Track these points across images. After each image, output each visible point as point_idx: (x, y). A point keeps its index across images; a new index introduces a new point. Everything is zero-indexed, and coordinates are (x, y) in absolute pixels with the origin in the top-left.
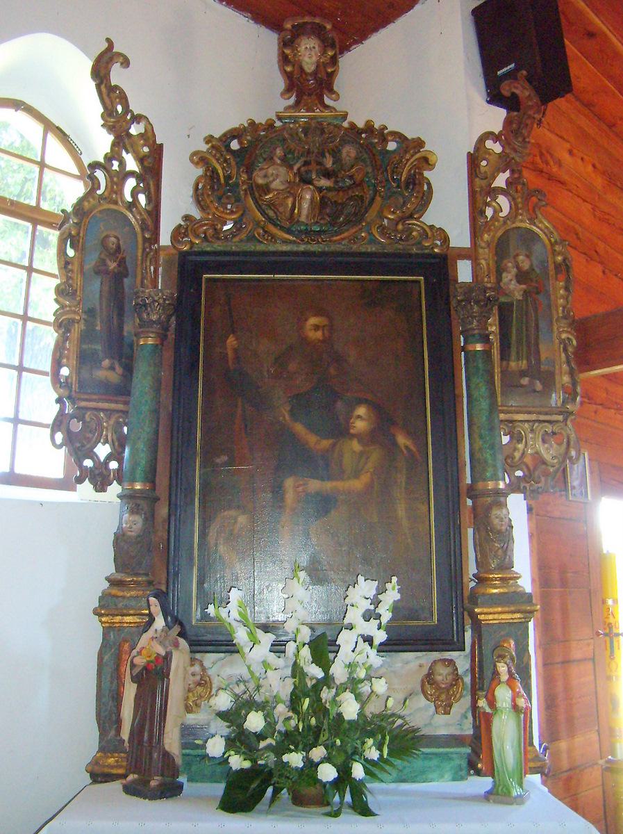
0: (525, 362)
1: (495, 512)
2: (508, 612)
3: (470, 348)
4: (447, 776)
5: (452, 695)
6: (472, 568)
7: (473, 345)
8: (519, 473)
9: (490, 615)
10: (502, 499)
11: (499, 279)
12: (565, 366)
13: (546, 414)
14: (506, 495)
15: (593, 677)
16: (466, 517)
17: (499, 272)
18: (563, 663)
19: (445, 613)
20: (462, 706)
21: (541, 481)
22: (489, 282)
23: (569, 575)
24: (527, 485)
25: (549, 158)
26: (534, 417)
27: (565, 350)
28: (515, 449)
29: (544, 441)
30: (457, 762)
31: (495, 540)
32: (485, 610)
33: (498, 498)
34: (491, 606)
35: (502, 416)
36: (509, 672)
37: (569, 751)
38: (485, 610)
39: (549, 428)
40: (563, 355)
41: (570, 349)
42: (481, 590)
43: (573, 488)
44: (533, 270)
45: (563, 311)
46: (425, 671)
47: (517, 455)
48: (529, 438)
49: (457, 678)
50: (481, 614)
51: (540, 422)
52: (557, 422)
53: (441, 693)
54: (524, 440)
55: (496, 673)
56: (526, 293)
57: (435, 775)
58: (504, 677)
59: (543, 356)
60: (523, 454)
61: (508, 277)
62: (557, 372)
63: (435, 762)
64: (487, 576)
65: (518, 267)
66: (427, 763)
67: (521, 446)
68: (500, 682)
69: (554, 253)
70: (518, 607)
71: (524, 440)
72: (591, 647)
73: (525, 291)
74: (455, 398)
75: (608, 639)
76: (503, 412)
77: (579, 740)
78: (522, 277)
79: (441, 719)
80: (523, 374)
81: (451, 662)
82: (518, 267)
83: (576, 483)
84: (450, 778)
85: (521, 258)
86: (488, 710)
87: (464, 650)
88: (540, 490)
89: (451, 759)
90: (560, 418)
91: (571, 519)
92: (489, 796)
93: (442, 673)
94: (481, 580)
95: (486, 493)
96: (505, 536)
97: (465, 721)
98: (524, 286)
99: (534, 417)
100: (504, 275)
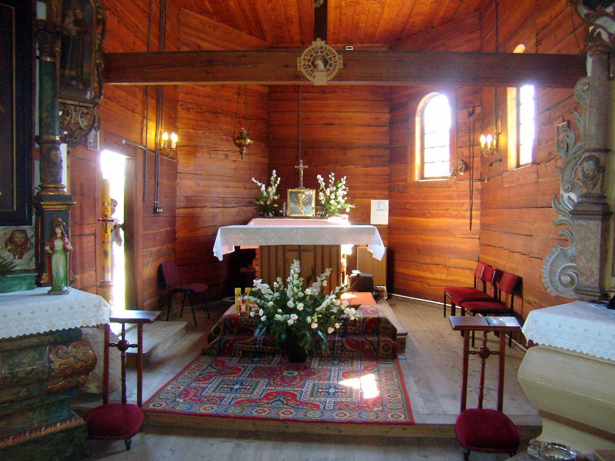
0: (75, 72)
1: (53, 152)
2: (59, 205)
3: (44, 58)
4: (24, 288)
5: (24, 249)
6: (37, 182)
7: (43, 59)
8: (66, 133)
9: (49, 206)
10: (57, 146)
11: (63, 22)
12: (96, 78)
13: (84, 102)
14: (60, 144)
15: (94, 244)
16: (35, 154)
17: (64, 16)
18: (80, 235)
19: (21, 206)
20: (30, 254)
21: (77, 139)
22: (59, 21)
23: (85, 190)
24: (70, 140)
25: (588, 200)
26: (77, 103)
27: (98, 69)
28: (65, 119)
29: (81, 117)
30: (30, 280)
31: (51, 167)
32: (47, 203)
33: (54, 146)
34: (49, 201)
35: (60, 100)
36: (62, 233)
37: (81, 280)
38: (47, 203)
39: (85, 111)
40: (96, 72)
41: (100, 69)
42: (44, 193)
43: (90, 143)
44: (84, 20)
45: (99, 47)
46: (8, 236)
47: (66, 122)
48: (73, 115)
49: (27, 239)
50: (44, 205)
51: (80, 106)
52: (90, 107)
53: (18, 248)
54: (70, 116)
55: (55, 234)
56: (79, 33)
57: (18, 288)
58: (59, 235)
59: (85, 71)
60: (69, 123)
61: (69, 21)
62: (92, 80)
63: (17, 282)
64: (47, 186)
65: (75, 15)
66: (13, 282)
67: (68, 118)
68: (56, 238)
69: (97, 12)
70: (65, 202)
71: (70, 116)
72: (94, 228)
73: (78, 31)
74: (32, 86)
75: (104, 223)
76: (60, 98)
77: (86, 275)
78: (77, 22)
79: (17, 261)
80: (72, 78)
81: (24, 231)
82: (75, 15)
83: (92, 141)
84: (25, 289)
85: (78, 11)
86: (50, 252)
87: (31, 225)
88: (77, 143)
89: (27, 279)
90: (92, 106)
91: (88, 160)
92: (49, 293)
93: (19, 238)
94: (43, 188)
95: (47, 142)
96: (57, 165)
97: (31, 262)
98: (77, 28)
99: (77, 103)
100: (67, 19)
